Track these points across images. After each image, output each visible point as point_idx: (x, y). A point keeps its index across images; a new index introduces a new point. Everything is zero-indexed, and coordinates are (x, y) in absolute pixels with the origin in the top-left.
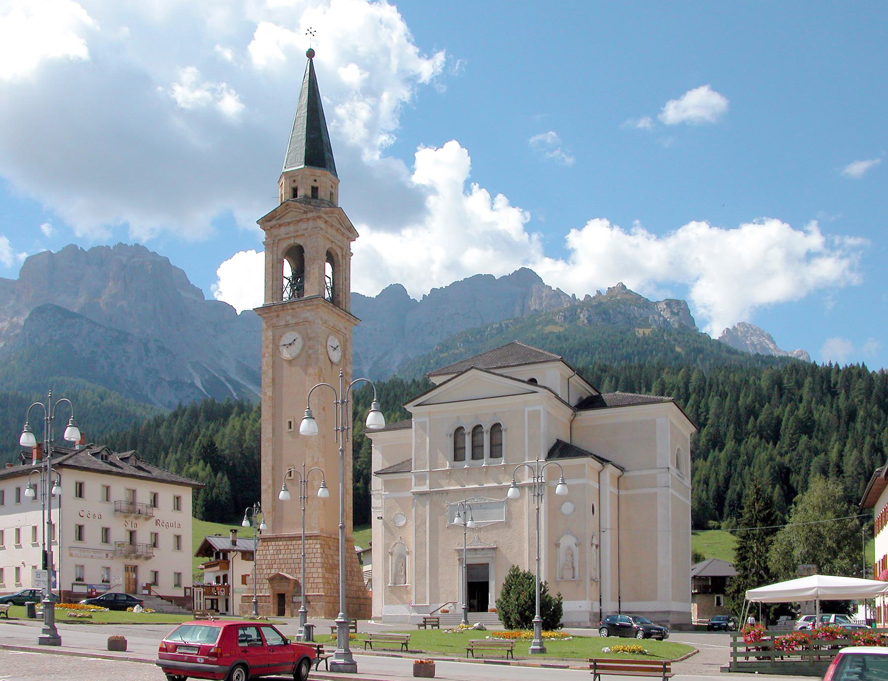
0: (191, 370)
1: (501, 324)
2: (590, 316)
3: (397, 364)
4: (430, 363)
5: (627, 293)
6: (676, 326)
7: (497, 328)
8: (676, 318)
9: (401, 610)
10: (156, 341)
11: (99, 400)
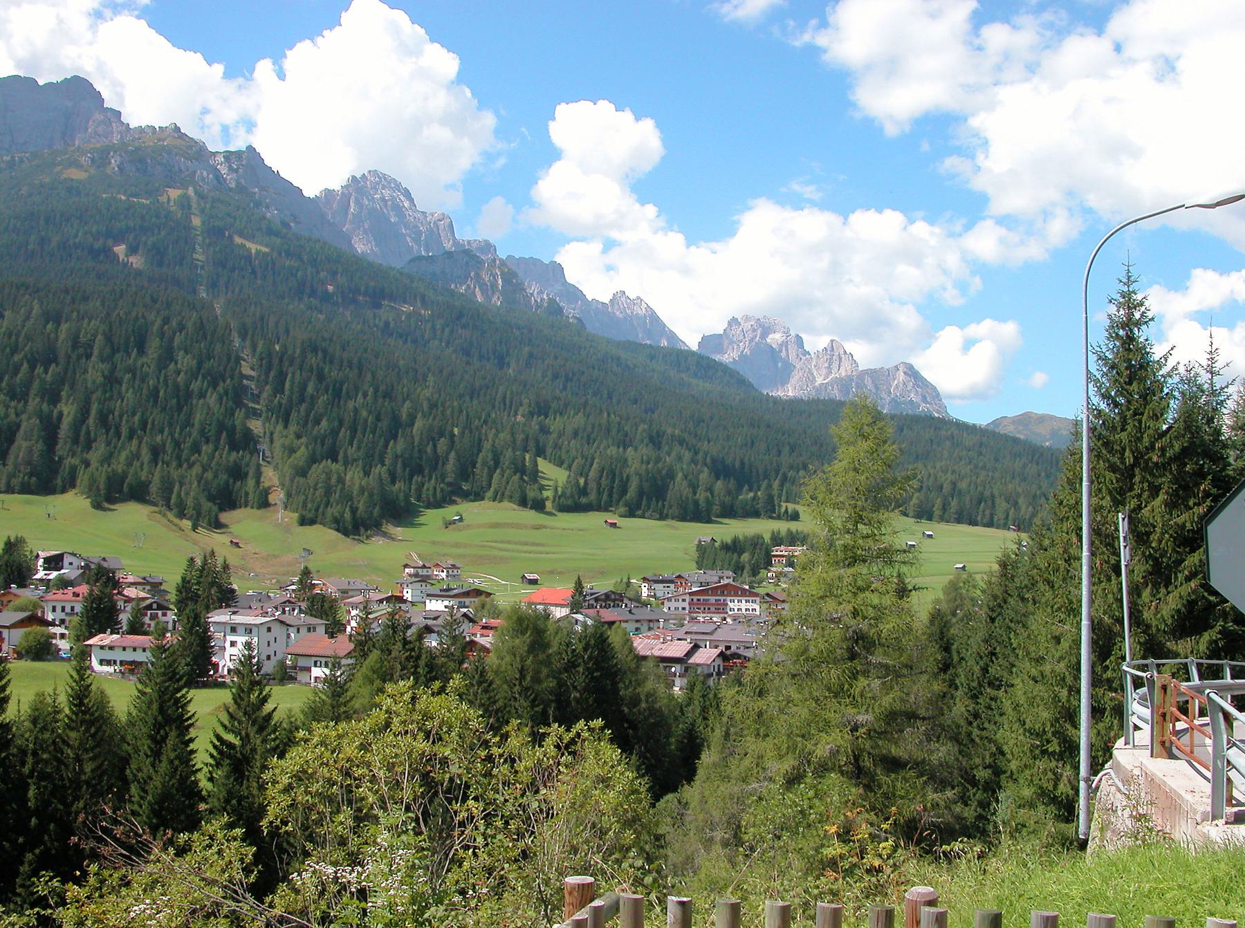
1: (13, 158)
2: (122, 163)
6: (233, 185)
9: (210, 829)
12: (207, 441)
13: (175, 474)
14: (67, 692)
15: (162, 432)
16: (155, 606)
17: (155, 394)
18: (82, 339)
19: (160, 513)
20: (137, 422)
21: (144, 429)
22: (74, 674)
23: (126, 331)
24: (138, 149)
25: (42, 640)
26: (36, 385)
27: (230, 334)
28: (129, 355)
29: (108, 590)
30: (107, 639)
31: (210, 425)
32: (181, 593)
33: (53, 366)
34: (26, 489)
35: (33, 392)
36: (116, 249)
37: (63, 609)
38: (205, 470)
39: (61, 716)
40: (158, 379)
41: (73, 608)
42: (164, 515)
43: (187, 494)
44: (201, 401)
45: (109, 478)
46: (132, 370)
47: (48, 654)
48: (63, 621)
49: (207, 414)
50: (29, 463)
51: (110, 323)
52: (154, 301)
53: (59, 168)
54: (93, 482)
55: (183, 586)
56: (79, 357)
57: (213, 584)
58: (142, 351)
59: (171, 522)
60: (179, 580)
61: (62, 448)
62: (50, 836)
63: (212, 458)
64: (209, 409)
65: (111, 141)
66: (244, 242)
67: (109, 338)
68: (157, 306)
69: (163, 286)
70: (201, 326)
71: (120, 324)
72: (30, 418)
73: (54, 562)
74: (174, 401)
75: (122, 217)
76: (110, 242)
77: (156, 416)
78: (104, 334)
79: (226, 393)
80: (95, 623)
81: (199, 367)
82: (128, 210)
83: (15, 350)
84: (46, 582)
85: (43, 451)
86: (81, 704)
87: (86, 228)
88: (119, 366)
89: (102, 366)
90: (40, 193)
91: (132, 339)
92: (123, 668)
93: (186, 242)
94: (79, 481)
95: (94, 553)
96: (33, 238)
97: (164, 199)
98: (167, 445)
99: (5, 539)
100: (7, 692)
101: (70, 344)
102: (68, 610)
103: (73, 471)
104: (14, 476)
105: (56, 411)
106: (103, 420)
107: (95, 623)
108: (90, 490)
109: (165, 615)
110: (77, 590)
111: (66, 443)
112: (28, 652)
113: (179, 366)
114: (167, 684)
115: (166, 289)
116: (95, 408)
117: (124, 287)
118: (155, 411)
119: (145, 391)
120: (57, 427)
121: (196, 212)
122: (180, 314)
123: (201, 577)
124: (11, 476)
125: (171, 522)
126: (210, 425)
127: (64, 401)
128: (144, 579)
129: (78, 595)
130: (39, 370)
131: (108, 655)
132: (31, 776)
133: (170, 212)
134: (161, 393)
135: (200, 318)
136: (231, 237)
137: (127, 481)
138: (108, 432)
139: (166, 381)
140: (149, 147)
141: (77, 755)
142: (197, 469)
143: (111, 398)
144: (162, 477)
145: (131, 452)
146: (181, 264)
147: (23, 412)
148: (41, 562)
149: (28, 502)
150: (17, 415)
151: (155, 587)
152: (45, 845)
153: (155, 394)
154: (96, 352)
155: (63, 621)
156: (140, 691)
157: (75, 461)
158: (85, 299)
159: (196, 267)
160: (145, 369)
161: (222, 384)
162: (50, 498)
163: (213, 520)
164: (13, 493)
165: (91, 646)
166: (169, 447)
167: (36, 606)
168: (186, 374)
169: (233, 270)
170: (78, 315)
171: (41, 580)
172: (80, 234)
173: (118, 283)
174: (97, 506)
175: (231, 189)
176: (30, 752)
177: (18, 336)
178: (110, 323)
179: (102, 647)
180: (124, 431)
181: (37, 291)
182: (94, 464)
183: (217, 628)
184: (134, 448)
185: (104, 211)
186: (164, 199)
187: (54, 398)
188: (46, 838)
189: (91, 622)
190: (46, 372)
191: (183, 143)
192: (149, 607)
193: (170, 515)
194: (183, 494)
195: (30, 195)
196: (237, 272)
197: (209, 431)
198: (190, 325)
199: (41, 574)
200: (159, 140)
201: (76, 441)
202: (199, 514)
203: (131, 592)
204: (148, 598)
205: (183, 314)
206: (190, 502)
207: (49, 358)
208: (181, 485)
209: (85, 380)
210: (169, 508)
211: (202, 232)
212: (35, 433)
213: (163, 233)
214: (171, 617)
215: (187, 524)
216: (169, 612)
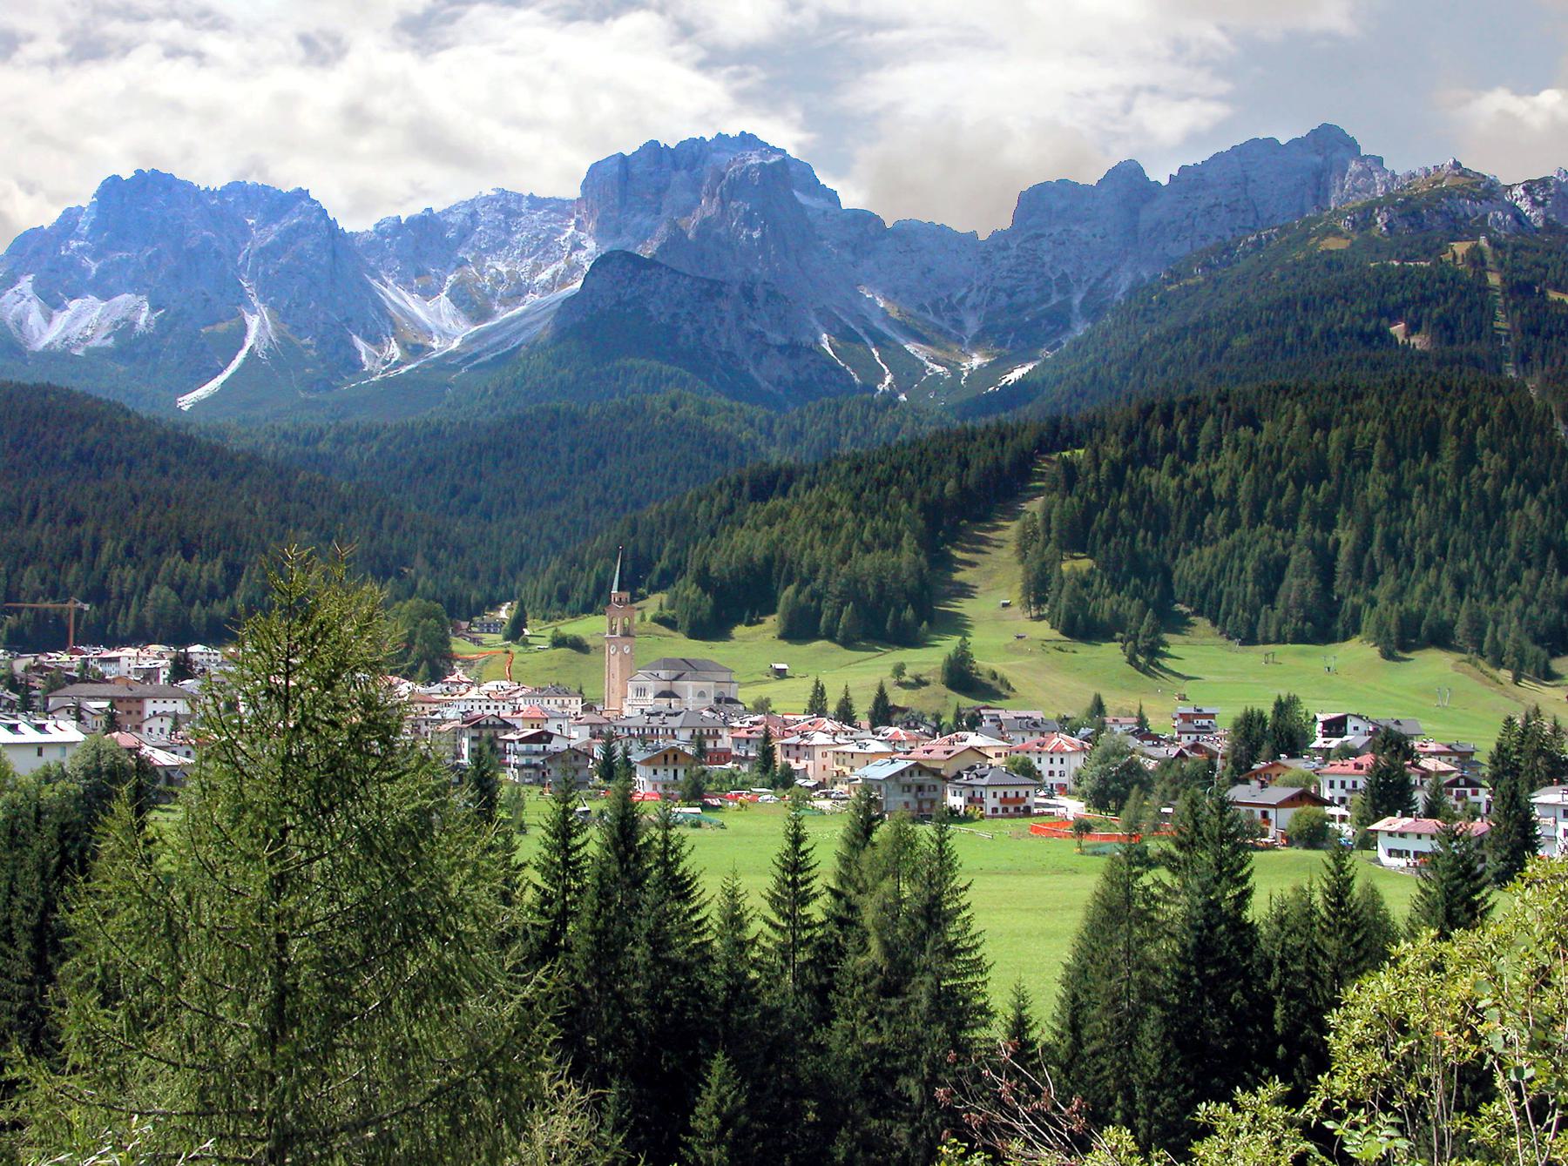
0: (815, 322)
1: (1259, 237)
2: (1390, 221)
3: (1123, 289)
4: (1151, 301)
5: (1461, 174)
6: (1540, 224)
7: (1253, 244)
8: (1540, 211)
10: (765, 283)
11: (669, 410)
12: (1529, 565)
13: (1488, 610)
14: (1321, 887)
15: (1467, 556)
16: (1462, 782)
17: (1454, 507)
18: (1358, 447)
19: (1469, 661)
20: (1433, 547)
21: (1443, 555)
22: (1331, 863)
23: (1413, 431)
24: (1409, 199)
25: (1316, 823)
26: (1305, 509)
27: (1551, 421)
28: (1418, 461)
29: (1397, 762)
30: (1397, 822)
31: (1531, 543)
32: (1497, 764)
33: (1325, 482)
34: (1299, 638)
35: (1302, 518)
36: (1393, 329)
37: (1343, 784)
38: (1527, 603)
39: (1316, 918)
40: (1458, 489)
41: (1354, 784)
42: (1475, 665)
43: (1505, 636)
44: (1517, 513)
45: (1401, 619)
46: (1423, 480)
47: (1324, 840)
48: (1342, 800)
49: (1527, 529)
50: (1302, 605)
51: (1392, 422)
52: (1446, 389)
53: (1314, 240)
54: (1381, 624)
55: (1499, 756)
56: (1356, 470)
57: (1540, 752)
58: (1434, 455)
59: (1485, 673)
60: (1493, 746)
61: (1340, 586)
62: (1301, 1071)
63: (1536, 586)
64: (1529, 521)
65: (1374, 196)
66: (1562, 296)
67: (1390, 442)
68: (1450, 395)
69: (1456, 368)
70: (1510, 414)
71: (1404, 423)
72: (1300, 550)
73: (1335, 727)
74: (1481, 515)
75: (1398, 287)
76: (1384, 321)
77: (1458, 536)
78: (1384, 436)
79: (1551, 499)
80: (1383, 802)
81: (1512, 469)
82: (1403, 278)
83: (1278, 467)
84: (1326, 754)
85: (1317, 589)
86: (1340, 903)
87: (1353, 308)
88: (1406, 476)
89: (1385, 478)
90: (1294, 274)
91: (1421, 440)
92: (1418, 862)
93: (1483, 308)
94: (1363, 626)
95: (1385, 715)
96: (1289, 331)
97: (1448, 257)
98: (1476, 573)
99: (1275, 699)
100: (1250, 884)
101: (1343, 454)
102: (1349, 785)
103: (1356, 612)
104: (1285, 622)
105: (1331, 540)
106: (1390, 545)
107: (1383, 802)
108: (1379, 635)
109: (1475, 793)
110: (1359, 760)
111: (1345, 578)
112: (1299, 838)
113: (1484, 470)
114: (1456, 882)
115: (1461, 371)
116: (1379, 531)
117: (1406, 376)
118: (1457, 530)
119: (1442, 506)
120: (1333, 558)
121: (1493, 267)
122: (1481, 401)
123: (1522, 743)
124: (1281, 622)
125: (1485, 673)
126: (1531, 543)
127: (1340, 526)
128: (1449, 747)
129: (1361, 767)
130: (1308, 490)
131: (1399, 844)
132: (1278, 991)
133: (1458, 272)
134: (1463, 507)
135: (1509, 404)
136: (1542, 293)
137: (1425, 622)
138: (1397, 561)
139: (1468, 493)
140: (1422, 193)
141: (1335, 969)
142: (1517, 602)
143: (1399, 518)
144: (1471, 615)
145: (1428, 584)
146: (1478, 338)
147: (1292, 543)
148: (1319, 726)
149: (1302, 653)
150: (1285, 547)
151: (1464, 757)
152: (1295, 1083)
153: (1454, 507)
154: (1376, 461)
155: (1342, 800)
156: (1423, 890)
157: (1359, 600)
158: (1358, 396)
159: (1499, 338)
160: (1440, 477)
161: (1544, 489)
162: (1331, 648)
163: (1541, 669)
164: (1285, 643)
165: (1376, 831)
166: (1478, 576)
167: (1309, 780)
168: (1495, 477)
169: (1550, 335)
170: (1351, 418)
171: (1319, 749)
172: (1346, 317)
173: (1399, 371)
174: (1388, 655)
175: (1537, 230)
176: (1276, 961)
177: (1280, 450)
178: (1392, 422)
179: (1391, 834)
180: (1418, 557)
181: (1300, 393)
182: (1382, 603)
183: (1545, 811)
184: (1432, 580)
185: (1374, 284)
186: (1448, 257)
187: (1329, 524)
188: (1296, 1072)
189: (1377, 801)
190: (1316, 491)
191: (1467, 180)
192: (1455, 783)
193: (1483, 664)
194: (1499, 636)
195: (1283, 279)
196: (1555, 337)
197: (1531, 551)
198: (1495, 414)
199: (1319, 742)
200: (1435, 183)
201: (1357, 575)
202: (1522, 661)
203: (1429, 764)
204: (1452, 772)
205: (1486, 402)
206: (1509, 646)
207: (1317, 472)
208: (1497, 623)
209: (1365, 497)
210: (1483, 657)
211: (1503, 293)
212: (1307, 568)
213: (1451, 301)
214: (1484, 796)
215: (1506, 675)
216: (1481, 791)
